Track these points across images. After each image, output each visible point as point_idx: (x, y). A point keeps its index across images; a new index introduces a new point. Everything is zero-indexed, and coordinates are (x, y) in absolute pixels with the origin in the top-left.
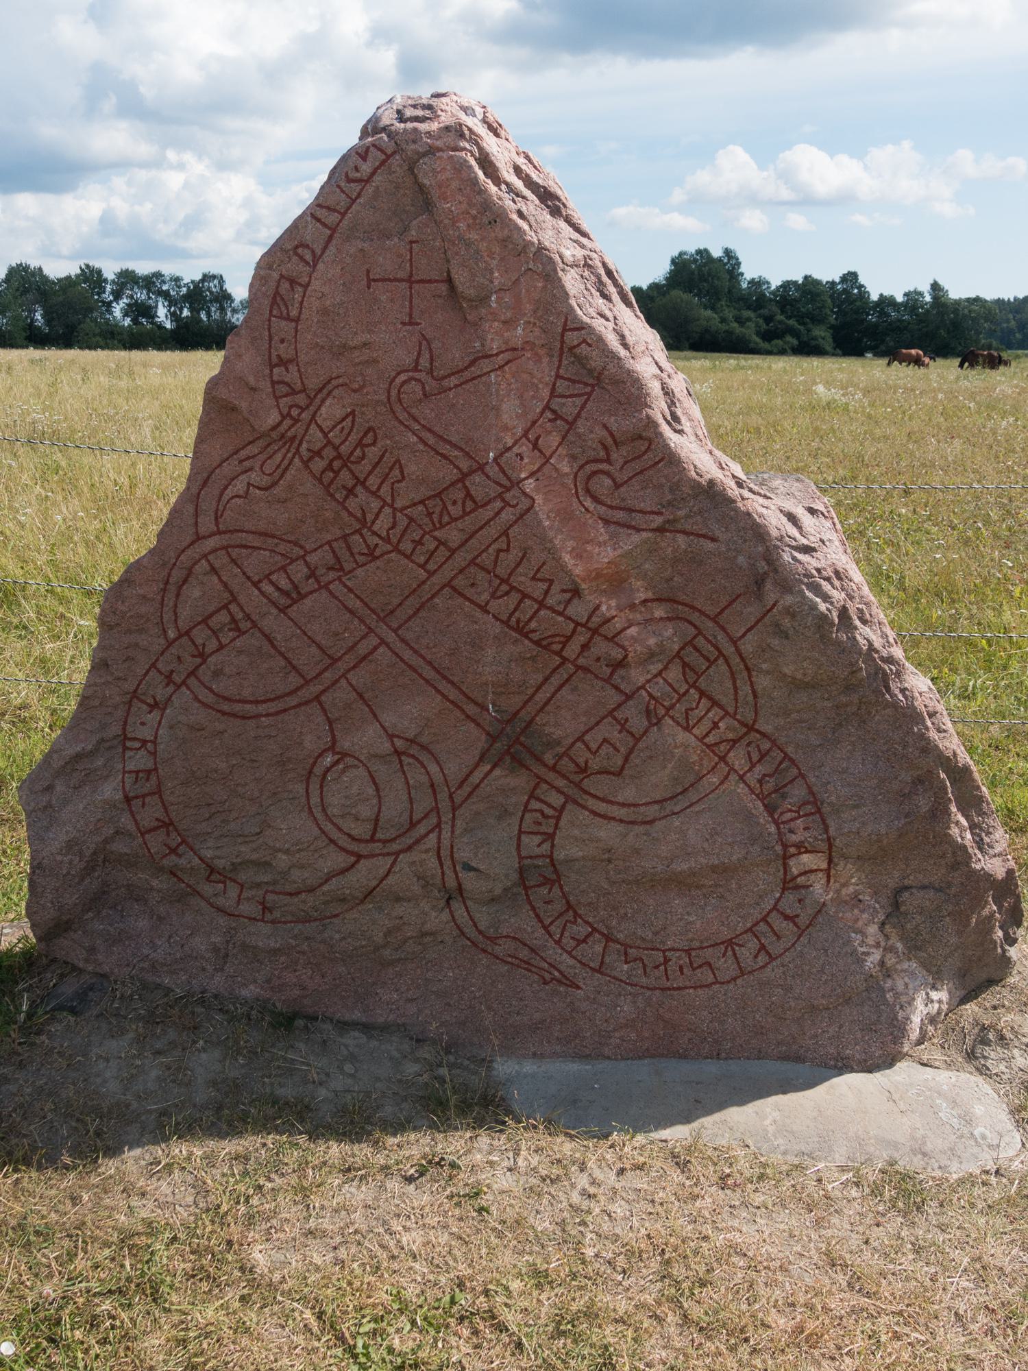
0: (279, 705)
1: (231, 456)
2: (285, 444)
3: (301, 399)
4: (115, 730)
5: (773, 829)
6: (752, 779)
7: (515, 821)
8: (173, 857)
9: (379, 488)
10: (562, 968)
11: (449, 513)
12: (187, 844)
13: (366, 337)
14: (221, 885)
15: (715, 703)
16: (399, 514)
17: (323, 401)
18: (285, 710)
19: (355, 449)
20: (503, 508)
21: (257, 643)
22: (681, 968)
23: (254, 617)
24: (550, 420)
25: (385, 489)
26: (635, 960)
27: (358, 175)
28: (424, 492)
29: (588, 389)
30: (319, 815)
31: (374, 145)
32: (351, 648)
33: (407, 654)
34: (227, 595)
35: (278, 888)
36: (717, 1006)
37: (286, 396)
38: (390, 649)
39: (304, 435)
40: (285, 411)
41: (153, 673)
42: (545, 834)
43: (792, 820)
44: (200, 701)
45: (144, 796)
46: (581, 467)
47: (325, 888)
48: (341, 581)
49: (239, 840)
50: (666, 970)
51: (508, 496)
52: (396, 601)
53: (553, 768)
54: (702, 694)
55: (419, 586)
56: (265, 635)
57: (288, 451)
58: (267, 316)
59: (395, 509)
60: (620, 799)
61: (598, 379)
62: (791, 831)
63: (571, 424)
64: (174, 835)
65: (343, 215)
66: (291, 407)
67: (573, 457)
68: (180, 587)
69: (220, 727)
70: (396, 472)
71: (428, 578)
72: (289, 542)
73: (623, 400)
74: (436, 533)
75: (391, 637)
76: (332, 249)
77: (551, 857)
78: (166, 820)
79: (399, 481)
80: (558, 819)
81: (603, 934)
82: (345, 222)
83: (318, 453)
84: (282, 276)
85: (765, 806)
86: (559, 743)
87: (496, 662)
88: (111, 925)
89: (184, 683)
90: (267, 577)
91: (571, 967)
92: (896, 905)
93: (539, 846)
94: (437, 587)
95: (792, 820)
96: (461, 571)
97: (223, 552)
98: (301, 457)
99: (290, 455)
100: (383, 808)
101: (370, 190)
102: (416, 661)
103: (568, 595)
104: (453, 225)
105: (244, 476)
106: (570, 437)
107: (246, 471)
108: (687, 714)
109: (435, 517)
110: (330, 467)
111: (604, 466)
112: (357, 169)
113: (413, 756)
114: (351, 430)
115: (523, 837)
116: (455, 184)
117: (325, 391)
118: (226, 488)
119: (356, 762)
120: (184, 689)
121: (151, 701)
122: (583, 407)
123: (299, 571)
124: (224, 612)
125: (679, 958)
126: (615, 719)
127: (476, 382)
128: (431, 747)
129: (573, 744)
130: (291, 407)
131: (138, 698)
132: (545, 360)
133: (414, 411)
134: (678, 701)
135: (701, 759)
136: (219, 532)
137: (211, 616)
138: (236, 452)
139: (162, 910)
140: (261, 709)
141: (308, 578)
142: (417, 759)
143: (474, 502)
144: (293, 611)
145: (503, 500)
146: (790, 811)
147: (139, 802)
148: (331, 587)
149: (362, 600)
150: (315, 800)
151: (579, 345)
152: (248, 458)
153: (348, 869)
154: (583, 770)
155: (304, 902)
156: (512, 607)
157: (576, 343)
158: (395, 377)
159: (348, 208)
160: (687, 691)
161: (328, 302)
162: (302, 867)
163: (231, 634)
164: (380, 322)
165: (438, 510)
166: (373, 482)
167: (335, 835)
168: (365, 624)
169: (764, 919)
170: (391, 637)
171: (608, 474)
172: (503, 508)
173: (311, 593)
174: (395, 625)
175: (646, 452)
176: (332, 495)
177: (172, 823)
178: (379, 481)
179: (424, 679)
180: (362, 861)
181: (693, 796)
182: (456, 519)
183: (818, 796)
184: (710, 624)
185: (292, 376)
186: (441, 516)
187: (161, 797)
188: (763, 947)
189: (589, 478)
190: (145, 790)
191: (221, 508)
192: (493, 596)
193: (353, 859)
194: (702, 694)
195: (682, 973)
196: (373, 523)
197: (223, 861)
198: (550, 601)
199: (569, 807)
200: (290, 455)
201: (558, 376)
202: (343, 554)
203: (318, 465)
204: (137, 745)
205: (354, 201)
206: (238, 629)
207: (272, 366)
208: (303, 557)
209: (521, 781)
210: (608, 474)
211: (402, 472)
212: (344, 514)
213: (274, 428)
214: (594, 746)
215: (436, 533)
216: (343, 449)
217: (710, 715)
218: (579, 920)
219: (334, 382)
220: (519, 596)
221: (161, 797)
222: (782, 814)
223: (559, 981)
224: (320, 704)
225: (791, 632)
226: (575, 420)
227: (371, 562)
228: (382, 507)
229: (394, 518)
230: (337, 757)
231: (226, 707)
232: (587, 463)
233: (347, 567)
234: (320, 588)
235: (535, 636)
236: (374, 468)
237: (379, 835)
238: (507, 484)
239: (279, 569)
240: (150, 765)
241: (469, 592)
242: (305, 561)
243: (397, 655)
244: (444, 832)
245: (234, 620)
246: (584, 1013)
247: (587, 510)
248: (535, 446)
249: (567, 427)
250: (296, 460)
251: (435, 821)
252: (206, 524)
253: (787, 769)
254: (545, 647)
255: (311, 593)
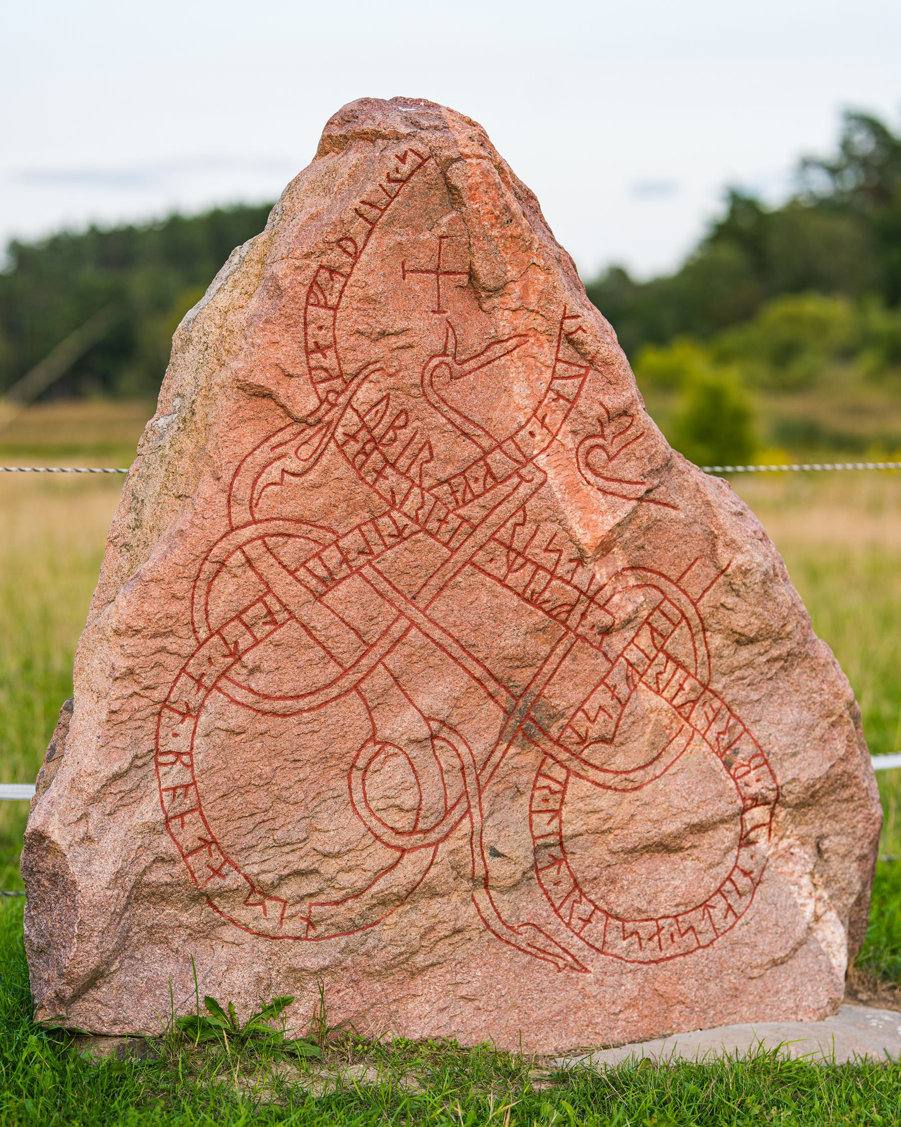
0: (320, 698)
1: (262, 443)
2: (321, 429)
3: (338, 384)
4: (149, 744)
5: (732, 784)
6: (711, 736)
7: (524, 800)
8: (217, 879)
9: (408, 470)
10: (573, 951)
11: (471, 491)
12: (232, 864)
13: (403, 324)
14: (260, 907)
15: (679, 665)
16: (427, 495)
17: (359, 386)
18: (326, 702)
19: (387, 432)
20: (520, 483)
21: (296, 635)
22: (672, 936)
23: (292, 608)
24: (554, 400)
25: (414, 470)
26: (632, 934)
27: (399, 176)
28: (450, 470)
29: (583, 371)
30: (364, 813)
31: (411, 150)
32: (385, 633)
33: (437, 634)
34: (262, 587)
35: (322, 898)
36: (702, 971)
37: (323, 381)
38: (420, 630)
39: (339, 420)
40: (323, 396)
41: (184, 678)
42: (553, 811)
43: (745, 774)
44: (238, 703)
45: (182, 815)
46: (581, 442)
47: (375, 889)
48: (370, 564)
49: (287, 849)
50: (659, 940)
51: (523, 472)
52: (421, 582)
53: (557, 742)
54: (669, 657)
55: (443, 565)
56: (303, 626)
57: (324, 436)
58: (304, 304)
59: (423, 489)
60: (613, 767)
61: (591, 362)
62: (747, 785)
63: (573, 402)
64: (216, 854)
65: (383, 211)
66: (328, 392)
67: (574, 432)
68: (210, 584)
69: (262, 727)
70: (425, 454)
71: (451, 556)
72: (321, 527)
73: (613, 380)
74: (460, 511)
75: (420, 618)
76: (373, 241)
77: (560, 834)
78: (209, 838)
79: (427, 462)
80: (564, 793)
81: (605, 912)
82: (385, 218)
83: (353, 437)
84: (321, 267)
85: (724, 763)
86: (563, 715)
87: (514, 633)
88: (136, 976)
89: (214, 685)
90: (303, 565)
91: (580, 949)
92: (820, 852)
93: (548, 824)
94: (459, 565)
95: (745, 774)
96: (481, 548)
97: (260, 542)
98: (336, 441)
99: (326, 440)
100: (424, 796)
101: (406, 189)
102: (447, 641)
103: (574, 564)
104: (480, 223)
105: (278, 463)
106: (572, 415)
107: (279, 458)
108: (657, 678)
109: (459, 495)
110: (362, 451)
111: (600, 441)
112: (397, 171)
113: (444, 739)
114: (385, 413)
115: (534, 816)
116: (483, 188)
117: (361, 376)
118: (259, 476)
119: (397, 750)
120: (215, 692)
121: (183, 709)
122: (581, 387)
123: (332, 556)
124: (260, 605)
125: (671, 925)
126: (606, 685)
127: (490, 366)
128: (459, 728)
129: (574, 715)
130: (328, 392)
131: (168, 707)
132: (546, 345)
133: (443, 393)
134: (649, 666)
135: (671, 722)
136: (255, 522)
137: (246, 610)
138: (267, 439)
139: (189, 949)
140: (303, 703)
141: (341, 563)
142: (448, 742)
143: (494, 478)
144: (329, 598)
145: (520, 476)
146: (743, 765)
147: (178, 821)
148: (363, 571)
149: (390, 583)
150: (358, 796)
151: (576, 331)
152: (281, 445)
153: (392, 867)
154: (583, 740)
155: (350, 909)
156: (527, 579)
157: (574, 329)
158: (428, 362)
159: (388, 205)
160: (657, 656)
161: (372, 292)
162: (350, 870)
163: (267, 627)
164: (414, 310)
165: (461, 488)
166: (403, 463)
167: (380, 830)
168: (396, 607)
169: (729, 878)
170: (420, 618)
171: (601, 447)
172: (520, 483)
173: (344, 578)
174: (422, 606)
175: (629, 427)
176: (362, 479)
177: (214, 841)
178: (409, 461)
179: (453, 658)
180: (406, 856)
181: (666, 760)
182: (479, 496)
183: (764, 749)
184: (674, 588)
185: (330, 361)
186: (464, 494)
187: (201, 814)
188: (730, 907)
189: (588, 453)
190: (185, 808)
191: (256, 496)
192: (510, 570)
193: (398, 854)
194: (669, 657)
195: (673, 941)
196: (402, 503)
197: (271, 875)
198: (560, 571)
199: (572, 779)
200: (326, 440)
201: (557, 360)
202: (373, 536)
203: (353, 447)
204: (171, 758)
205: (393, 199)
206: (274, 622)
207: (308, 353)
208: (336, 542)
209: (530, 758)
210: (601, 447)
211: (431, 453)
212: (375, 497)
213: (313, 413)
214: (592, 714)
215: (460, 511)
216: (377, 432)
217: (676, 677)
218: (584, 899)
219: (371, 367)
220: (533, 567)
221: (201, 814)
222: (736, 769)
223: (572, 968)
224: (359, 693)
225: (742, 589)
226: (575, 399)
227: (400, 542)
228: (411, 488)
229: (423, 498)
230: (378, 747)
231: (267, 706)
232: (587, 438)
233: (376, 550)
234: (353, 573)
235: (546, 606)
236: (405, 449)
237: (421, 826)
238: (521, 459)
239: (314, 557)
240: (188, 779)
241: (489, 567)
242: (338, 547)
243: (427, 635)
244: (475, 816)
245: (270, 613)
246: (595, 997)
247: (589, 483)
248: (543, 425)
249: (569, 406)
250: (332, 445)
251: (466, 805)
252: (241, 514)
253: (734, 726)
254: (554, 617)
255: (344, 578)
